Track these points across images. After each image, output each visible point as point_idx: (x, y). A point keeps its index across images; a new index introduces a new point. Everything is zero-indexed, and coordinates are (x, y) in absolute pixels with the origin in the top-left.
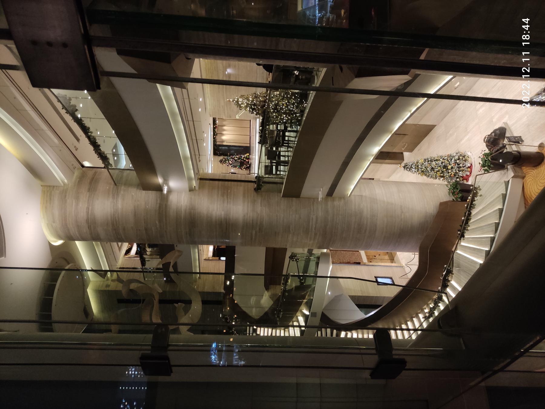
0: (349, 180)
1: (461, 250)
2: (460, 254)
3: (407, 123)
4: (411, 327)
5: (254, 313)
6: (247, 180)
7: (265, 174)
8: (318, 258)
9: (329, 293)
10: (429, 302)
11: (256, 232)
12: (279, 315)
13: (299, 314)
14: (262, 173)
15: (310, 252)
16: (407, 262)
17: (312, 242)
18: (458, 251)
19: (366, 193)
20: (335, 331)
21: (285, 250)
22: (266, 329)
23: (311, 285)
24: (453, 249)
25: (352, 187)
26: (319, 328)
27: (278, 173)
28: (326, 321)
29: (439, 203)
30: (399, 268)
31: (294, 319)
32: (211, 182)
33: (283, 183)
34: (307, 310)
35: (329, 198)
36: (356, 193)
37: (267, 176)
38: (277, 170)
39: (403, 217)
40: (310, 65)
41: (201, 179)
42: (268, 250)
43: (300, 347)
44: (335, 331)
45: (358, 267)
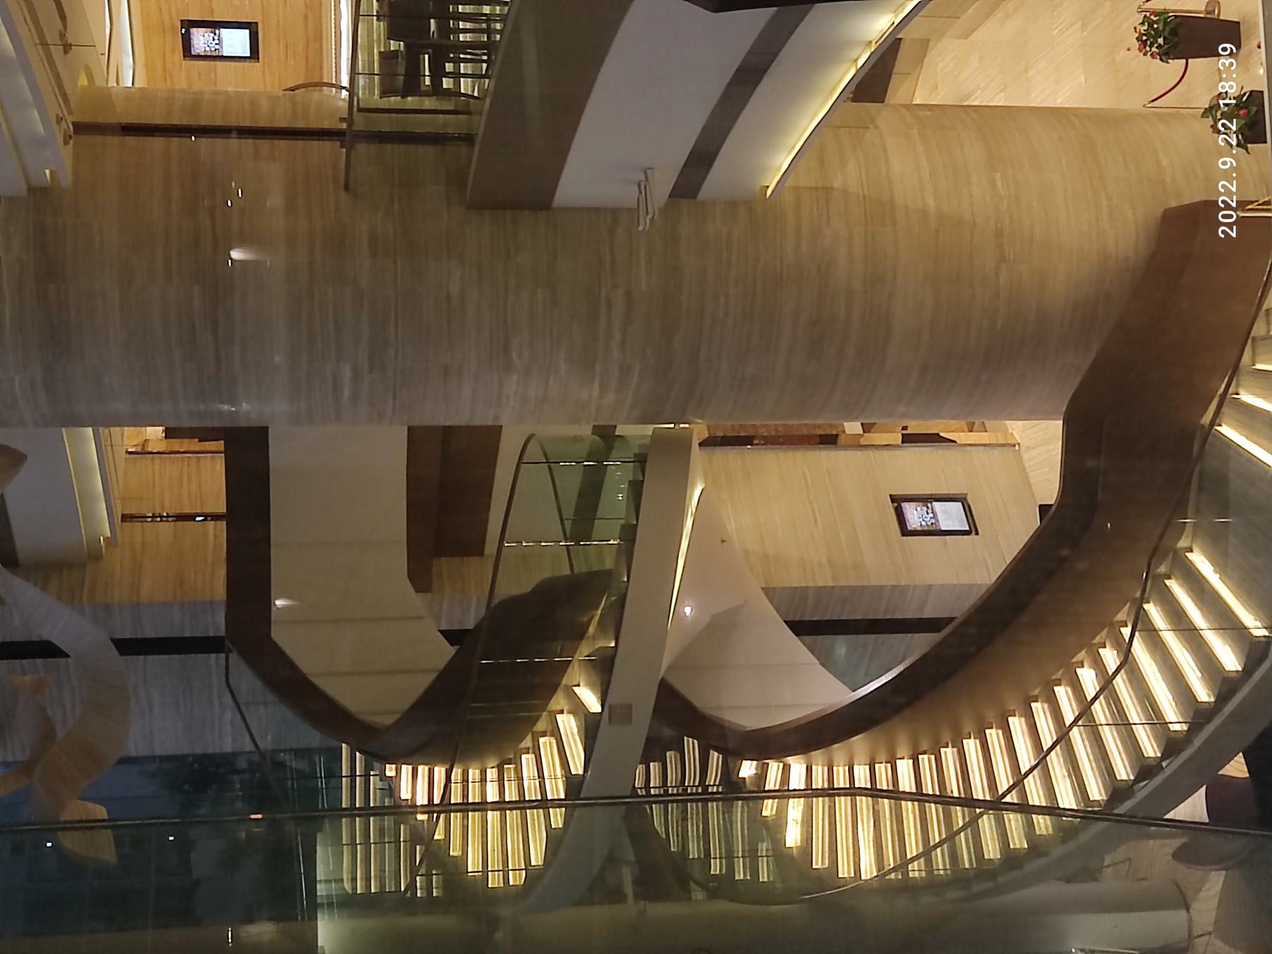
0: (772, 131)
2: (1229, 444)
6: (300, 124)
7: (385, 93)
8: (641, 461)
9: (688, 610)
10: (1097, 640)
12: (478, 700)
13: (559, 701)
14: (369, 93)
15: (606, 434)
16: (1025, 456)
17: (610, 398)
18: (1226, 430)
19: (849, 176)
20: (715, 758)
21: (494, 433)
22: (423, 770)
23: (608, 574)
24: (1206, 419)
25: (784, 161)
26: (653, 750)
27: (447, 83)
28: (677, 717)
29: (1159, 213)
30: (996, 452)
31: (541, 726)
32: (131, 141)
33: (481, 113)
34: (591, 685)
35: (685, 204)
36: (806, 179)
37: (394, 102)
38: (438, 72)
39: (1003, 278)
41: (80, 128)
42: (416, 437)
44: (715, 758)
45: (825, 456)
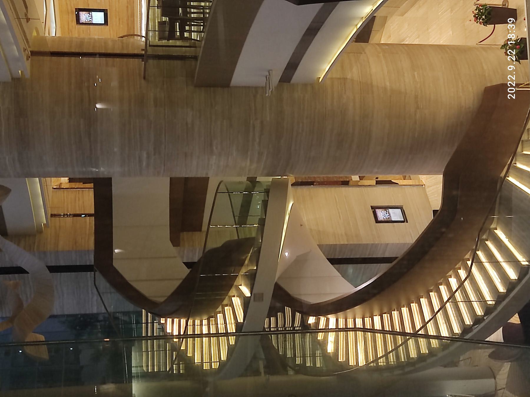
0: (322, 54)
1: (515, 177)
2: (512, 185)
3: (329, 76)
4: (378, 326)
5: (158, 290)
6: (125, 52)
7: (160, 39)
8: (267, 192)
9: (287, 254)
10: (457, 266)
11: (148, 154)
12: (199, 291)
13: (233, 292)
14: (154, 39)
15: (253, 181)
17: (254, 166)
18: (511, 179)
19: (354, 73)
20: (298, 315)
21: (206, 180)
22: (176, 320)
23: (253, 239)
24: (503, 175)
25: (327, 67)
26: (272, 312)
27: (186, 35)
28: (282, 299)
31: (225, 302)
32: (54, 58)
33: (200, 47)
34: (246, 285)
35: (285, 85)
37: (164, 42)
39: (418, 116)
40: (164, 42)
41: (33, 53)
42: (173, 182)
43: (255, 332)
44: (298, 315)
